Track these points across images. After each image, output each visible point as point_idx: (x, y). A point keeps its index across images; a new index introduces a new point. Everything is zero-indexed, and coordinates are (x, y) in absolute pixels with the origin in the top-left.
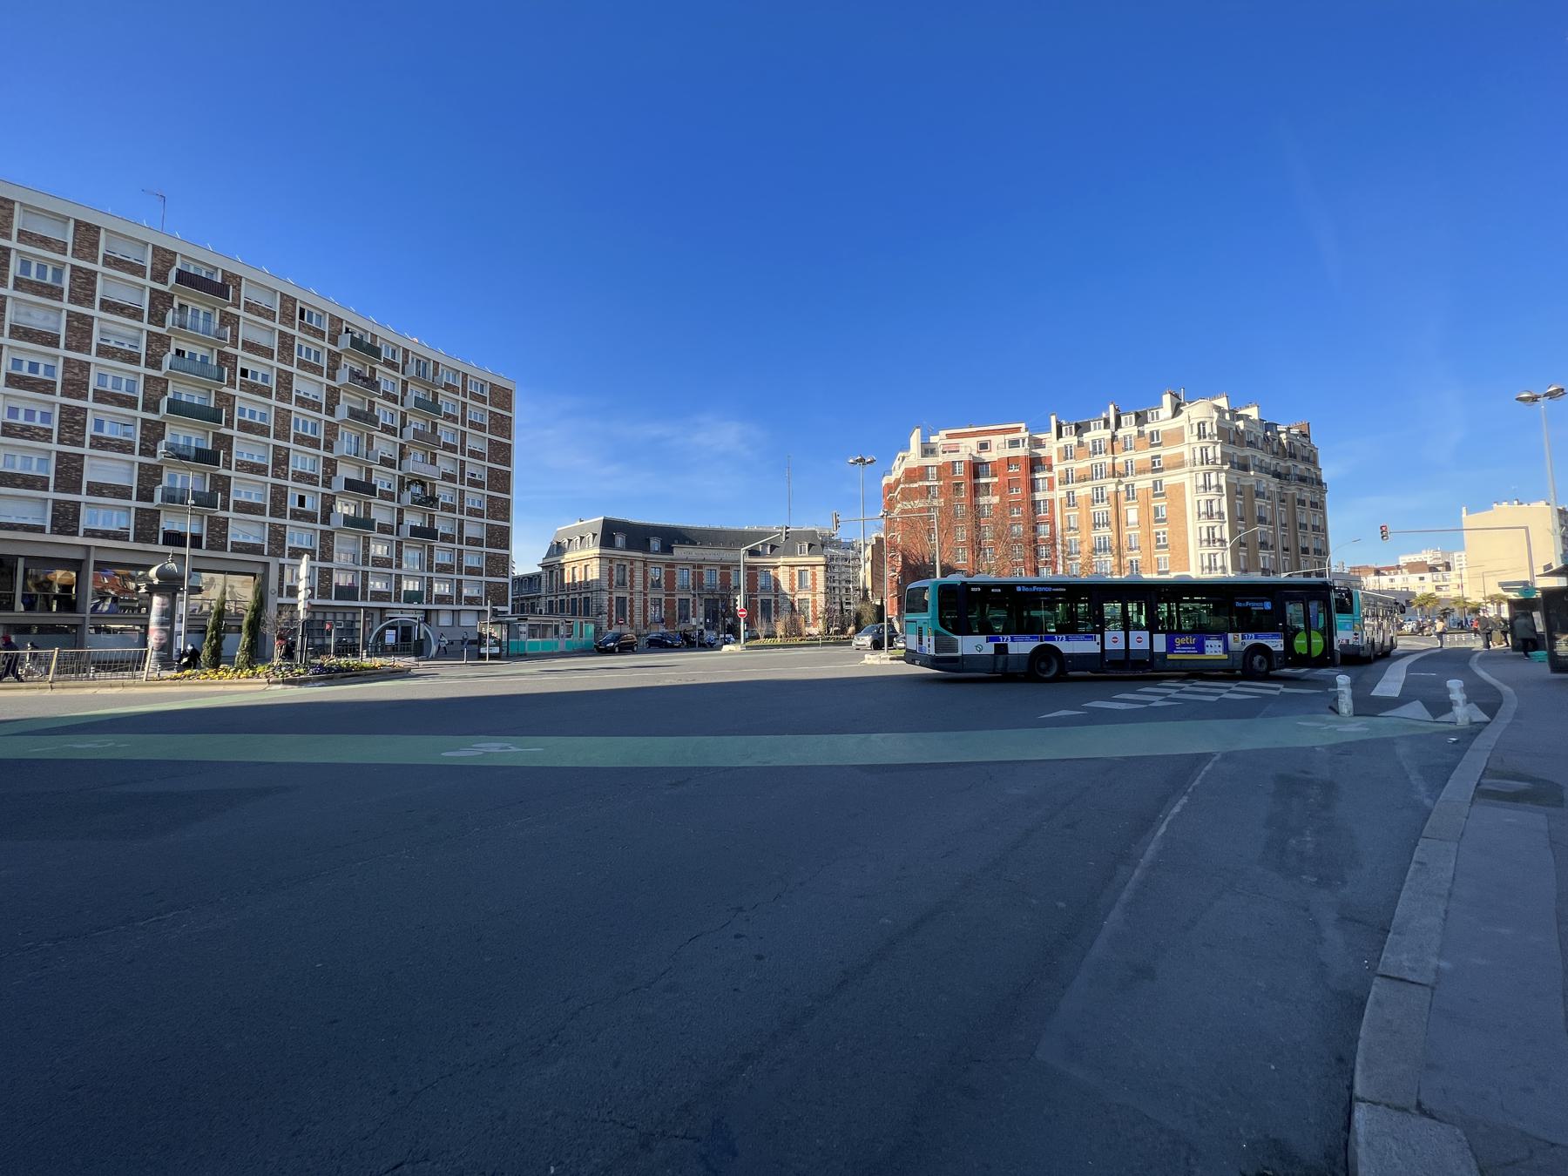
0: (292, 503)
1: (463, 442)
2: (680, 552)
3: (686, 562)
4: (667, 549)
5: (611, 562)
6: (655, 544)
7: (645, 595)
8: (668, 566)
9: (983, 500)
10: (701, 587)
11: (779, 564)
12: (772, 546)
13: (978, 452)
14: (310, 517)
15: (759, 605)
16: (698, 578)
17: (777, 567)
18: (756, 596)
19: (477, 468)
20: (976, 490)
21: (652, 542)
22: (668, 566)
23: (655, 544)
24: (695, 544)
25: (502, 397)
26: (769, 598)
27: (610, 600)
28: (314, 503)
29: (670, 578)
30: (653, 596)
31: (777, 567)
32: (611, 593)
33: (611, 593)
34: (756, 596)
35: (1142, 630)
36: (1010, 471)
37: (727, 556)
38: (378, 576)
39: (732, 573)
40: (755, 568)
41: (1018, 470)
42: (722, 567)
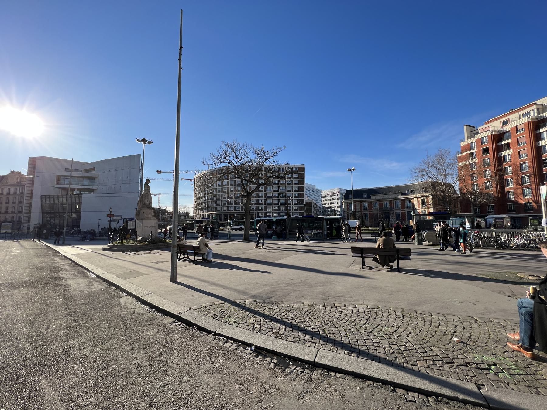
0: (260, 202)
1: (292, 182)
2: (373, 197)
3: (376, 200)
4: (369, 197)
5: (348, 203)
6: (365, 196)
7: (361, 212)
8: (369, 202)
9: (504, 153)
10: (382, 208)
11: (413, 197)
12: (411, 190)
13: (501, 127)
14: (262, 204)
15: (406, 214)
16: (381, 205)
17: (413, 198)
18: (405, 210)
19: (296, 187)
20: (499, 149)
21: (364, 195)
22: (369, 202)
23: (365, 196)
24: (380, 193)
25: (301, 169)
26: (399, 211)
27: (348, 214)
28: (534, 165)
29: (370, 206)
30: (396, 211)
31: (413, 198)
32: (348, 212)
33: (348, 212)
34: (405, 210)
35: (80, 217)
36: (517, 134)
37: (392, 196)
38: (275, 213)
39: (406, 202)
40: (404, 200)
41: (523, 132)
42: (380, 201)
